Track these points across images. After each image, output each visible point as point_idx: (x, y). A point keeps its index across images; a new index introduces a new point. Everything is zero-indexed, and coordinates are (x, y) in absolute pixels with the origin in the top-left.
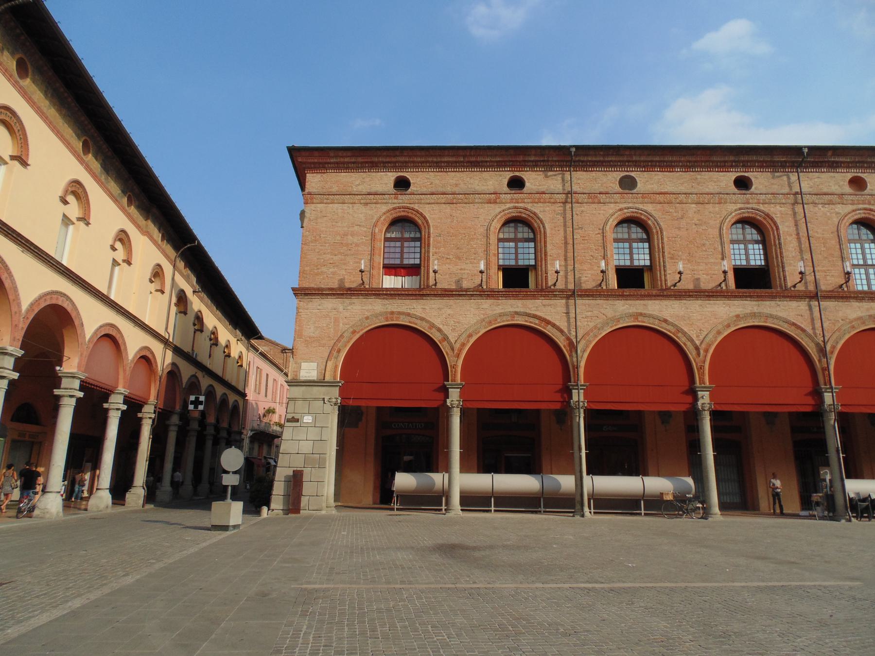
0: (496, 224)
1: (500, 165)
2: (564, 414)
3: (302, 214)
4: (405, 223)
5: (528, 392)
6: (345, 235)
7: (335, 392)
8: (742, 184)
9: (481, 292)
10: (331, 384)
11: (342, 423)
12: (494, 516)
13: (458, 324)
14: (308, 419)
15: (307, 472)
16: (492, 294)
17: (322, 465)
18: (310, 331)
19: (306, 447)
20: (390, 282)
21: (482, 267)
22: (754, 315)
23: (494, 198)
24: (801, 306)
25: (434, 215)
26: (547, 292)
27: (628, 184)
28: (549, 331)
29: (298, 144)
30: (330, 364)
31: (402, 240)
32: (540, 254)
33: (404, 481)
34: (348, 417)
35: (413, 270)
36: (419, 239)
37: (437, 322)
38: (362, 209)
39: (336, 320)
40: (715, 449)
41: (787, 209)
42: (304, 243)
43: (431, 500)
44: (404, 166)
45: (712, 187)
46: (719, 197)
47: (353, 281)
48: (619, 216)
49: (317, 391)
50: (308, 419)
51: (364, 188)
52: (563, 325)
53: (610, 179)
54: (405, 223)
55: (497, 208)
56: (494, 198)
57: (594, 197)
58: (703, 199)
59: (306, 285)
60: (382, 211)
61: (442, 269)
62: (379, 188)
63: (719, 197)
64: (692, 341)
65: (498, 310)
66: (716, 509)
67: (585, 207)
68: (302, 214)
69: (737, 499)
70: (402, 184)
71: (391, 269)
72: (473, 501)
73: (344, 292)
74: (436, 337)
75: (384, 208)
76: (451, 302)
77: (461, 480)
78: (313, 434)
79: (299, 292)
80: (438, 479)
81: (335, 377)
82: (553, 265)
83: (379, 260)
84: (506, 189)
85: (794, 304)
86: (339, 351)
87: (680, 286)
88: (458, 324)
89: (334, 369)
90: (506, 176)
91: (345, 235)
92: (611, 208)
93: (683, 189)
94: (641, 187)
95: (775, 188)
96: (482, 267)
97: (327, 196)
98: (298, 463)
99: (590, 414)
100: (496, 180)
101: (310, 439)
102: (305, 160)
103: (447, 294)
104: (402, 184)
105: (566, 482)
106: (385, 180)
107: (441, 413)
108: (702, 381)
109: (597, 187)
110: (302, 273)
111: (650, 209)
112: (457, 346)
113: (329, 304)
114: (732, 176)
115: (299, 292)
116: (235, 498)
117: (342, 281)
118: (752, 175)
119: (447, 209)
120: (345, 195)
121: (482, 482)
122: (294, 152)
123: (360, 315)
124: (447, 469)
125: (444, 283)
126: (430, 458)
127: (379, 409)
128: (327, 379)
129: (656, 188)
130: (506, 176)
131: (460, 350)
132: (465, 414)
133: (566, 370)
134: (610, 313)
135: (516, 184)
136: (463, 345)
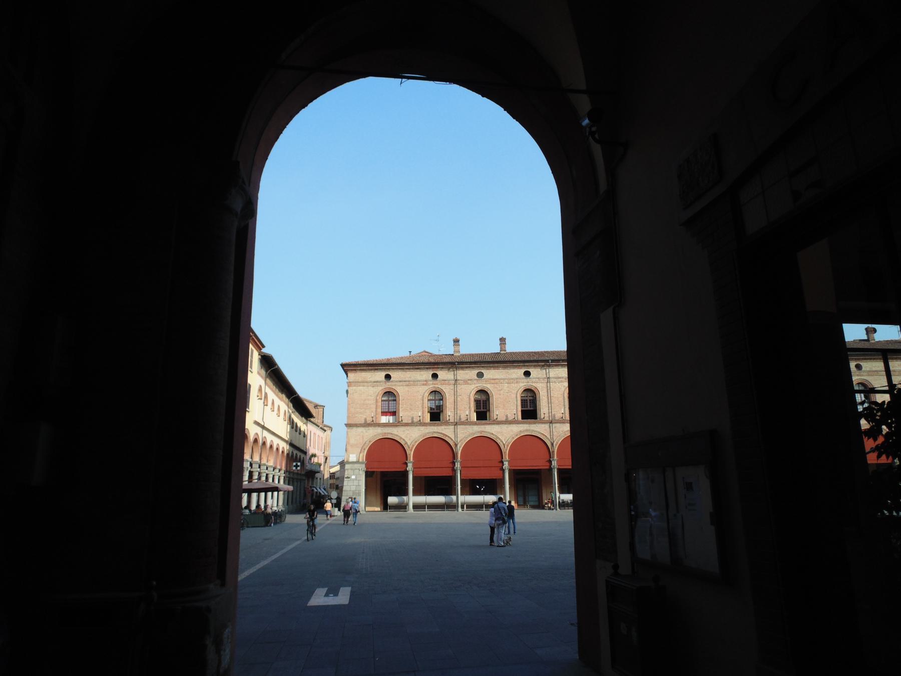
0: (427, 394)
2: (550, 470)
3: (347, 391)
4: (390, 395)
5: (536, 463)
7: (364, 466)
8: (527, 374)
9: (421, 424)
10: (362, 463)
12: (427, 512)
13: (411, 437)
14: (353, 477)
16: (425, 424)
17: (359, 494)
18: (352, 441)
19: (353, 488)
20: (384, 419)
22: (527, 430)
23: (426, 383)
24: (547, 426)
26: (447, 423)
27: (480, 375)
28: (447, 439)
31: (389, 401)
33: (392, 500)
34: (369, 474)
35: (394, 414)
37: (403, 437)
40: (414, 485)
41: (544, 385)
42: (349, 404)
43: (402, 507)
45: (514, 376)
46: (517, 381)
47: (369, 420)
49: (356, 466)
51: (373, 379)
53: (472, 373)
54: (390, 395)
56: (426, 383)
57: (466, 382)
58: (510, 381)
60: (380, 389)
61: (404, 414)
63: (517, 381)
65: (427, 431)
67: (463, 386)
69: (537, 503)
70: (388, 377)
71: (384, 413)
72: (417, 507)
73: (366, 425)
74: (403, 443)
75: (381, 388)
76: (408, 428)
77: (412, 499)
78: (356, 483)
79: (347, 425)
80: (454, 498)
83: (380, 411)
85: (543, 425)
88: (411, 437)
89: (363, 457)
90: (431, 372)
92: (473, 386)
93: (503, 377)
95: (540, 376)
97: (356, 383)
99: (559, 470)
100: (426, 375)
102: (347, 368)
103: (407, 425)
104: (388, 377)
106: (380, 375)
107: (405, 473)
109: (467, 377)
110: (348, 417)
111: (488, 387)
113: (360, 430)
114: (523, 370)
115: (347, 425)
117: (365, 420)
119: (407, 388)
120: (364, 382)
122: (343, 366)
123: (372, 434)
124: (455, 493)
125: (502, 418)
126: (402, 491)
129: (491, 377)
130: (431, 372)
134: (471, 431)
135: (435, 376)
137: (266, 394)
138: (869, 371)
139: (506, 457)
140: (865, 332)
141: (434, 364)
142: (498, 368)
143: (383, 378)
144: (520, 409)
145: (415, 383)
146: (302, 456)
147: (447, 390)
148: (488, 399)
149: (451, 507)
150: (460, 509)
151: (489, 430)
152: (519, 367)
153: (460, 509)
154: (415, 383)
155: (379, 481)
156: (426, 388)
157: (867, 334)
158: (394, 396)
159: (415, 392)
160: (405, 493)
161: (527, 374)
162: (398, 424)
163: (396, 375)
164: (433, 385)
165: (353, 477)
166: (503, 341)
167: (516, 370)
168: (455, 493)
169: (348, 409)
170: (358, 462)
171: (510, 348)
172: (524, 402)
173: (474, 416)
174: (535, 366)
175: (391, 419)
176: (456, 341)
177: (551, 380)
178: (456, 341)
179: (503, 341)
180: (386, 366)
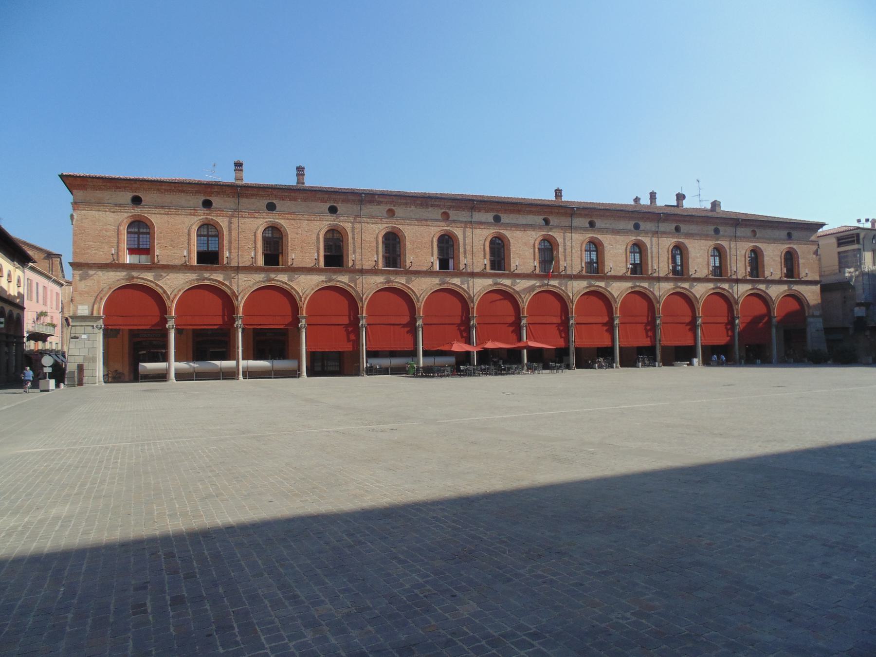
1: (539, 213)
3: (72, 216)
6: (101, 230)
9: (185, 268)
11: (106, 336)
15: (85, 364)
17: (94, 360)
19: (85, 352)
21: (185, 254)
25: (158, 220)
29: (65, 173)
30: (96, 306)
32: (220, 244)
34: (109, 334)
35: (147, 251)
36: (148, 233)
38: (112, 215)
39: (98, 282)
42: (75, 235)
43: (162, 377)
44: (137, 190)
50: (84, 337)
55: (196, 218)
59: (77, 261)
62: (122, 202)
64: (298, 293)
66: (305, 374)
68: (72, 216)
75: (126, 215)
77: (174, 365)
78: (88, 344)
81: (99, 313)
82: (515, 262)
84: (201, 206)
86: (101, 299)
87: (516, 272)
89: (100, 309)
91: (101, 230)
94: (503, 221)
96: (185, 254)
98: (80, 360)
101: (88, 349)
105: (230, 364)
108: (419, 314)
110: (75, 253)
112: (172, 297)
116: (50, 378)
121: (183, 365)
125: (163, 262)
127: (130, 330)
128: (95, 314)
131: (174, 298)
132: (179, 332)
133: (163, 309)
136: (176, 295)
137: (434, 518)
140: (675, 198)
141: (207, 193)
143: (129, 201)
144: (322, 253)
146: (16, 312)
148: (282, 238)
149: (230, 375)
150: (241, 377)
152: (323, 201)
153: (241, 377)
155: (126, 343)
157: (678, 199)
158: (147, 226)
159: (177, 234)
160: (165, 358)
162: (152, 267)
165: (84, 337)
166: (300, 170)
168: (165, 358)
169: (75, 242)
170: (91, 318)
171: (310, 181)
172: (327, 247)
173: (261, 262)
175: (144, 259)
176: (238, 165)
178: (238, 165)
179: (300, 170)
180: (136, 190)
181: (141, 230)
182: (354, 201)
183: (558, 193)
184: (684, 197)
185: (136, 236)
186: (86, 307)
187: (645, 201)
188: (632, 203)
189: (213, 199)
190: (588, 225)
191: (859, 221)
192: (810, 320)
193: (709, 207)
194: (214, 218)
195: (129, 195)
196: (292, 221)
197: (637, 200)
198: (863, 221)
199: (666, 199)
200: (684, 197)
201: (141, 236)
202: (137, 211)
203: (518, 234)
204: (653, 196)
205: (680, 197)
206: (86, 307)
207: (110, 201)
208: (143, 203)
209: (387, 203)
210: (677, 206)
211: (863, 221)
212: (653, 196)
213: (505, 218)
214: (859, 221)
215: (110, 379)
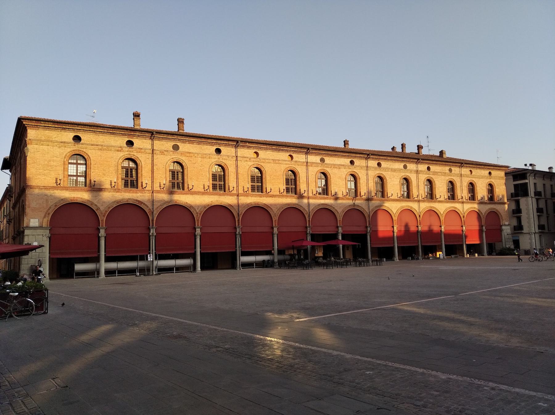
22: (472, 208)
23: (120, 149)
36: (177, 172)
45: (207, 152)
46: (209, 156)
48: (377, 175)
51: (59, 139)
52: (417, 210)
63: (209, 156)
65: (212, 200)
67: (158, 156)
70: (77, 139)
72: (109, 273)
75: (69, 150)
77: (104, 266)
85: (231, 197)
89: (46, 222)
95: (229, 154)
100: (122, 141)
106: (69, 136)
109: (163, 148)
111: (184, 160)
118: (453, 168)
119: (99, 153)
120: (49, 141)
129: (187, 150)
138: (434, 172)
139: (198, 224)
140: (417, 148)
142: (192, 142)
145: (108, 148)
147: (144, 161)
149: (145, 271)
151: (181, 198)
152: (212, 144)
154: (108, 148)
156: (250, 163)
157: (418, 149)
160: (96, 260)
161: (218, 151)
163: (86, 137)
164: (127, 152)
167: (209, 147)
168: (96, 260)
170: (41, 227)
174: (226, 145)
176: (136, 116)
177: (239, 159)
178: (136, 116)
179: (180, 121)
181: (79, 162)
182: (232, 145)
183: (346, 143)
184: (422, 147)
185: (75, 166)
186: (37, 220)
187: (399, 149)
188: (391, 150)
189: (134, 140)
190: (376, 166)
191: (526, 165)
192: (503, 227)
193: (438, 154)
194: (135, 154)
195: (72, 135)
196: (190, 159)
197: (393, 148)
198: (528, 165)
199: (411, 149)
200: (422, 147)
201: (79, 166)
202: (77, 147)
203: (335, 171)
204: (403, 146)
205: (419, 147)
206: (37, 220)
207: (56, 139)
208: (82, 142)
209: (254, 148)
210: (418, 153)
211: (528, 165)
212: (403, 146)
213: (384, 164)
214: (526, 165)
215: (55, 276)
